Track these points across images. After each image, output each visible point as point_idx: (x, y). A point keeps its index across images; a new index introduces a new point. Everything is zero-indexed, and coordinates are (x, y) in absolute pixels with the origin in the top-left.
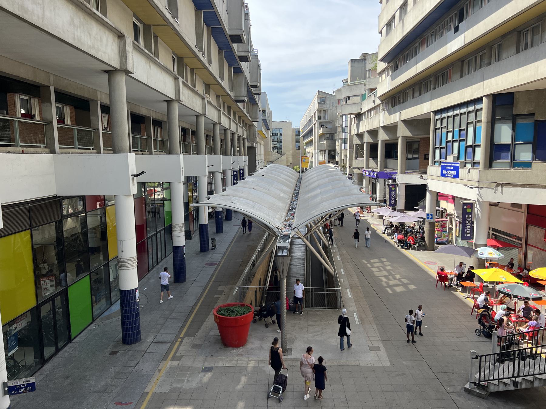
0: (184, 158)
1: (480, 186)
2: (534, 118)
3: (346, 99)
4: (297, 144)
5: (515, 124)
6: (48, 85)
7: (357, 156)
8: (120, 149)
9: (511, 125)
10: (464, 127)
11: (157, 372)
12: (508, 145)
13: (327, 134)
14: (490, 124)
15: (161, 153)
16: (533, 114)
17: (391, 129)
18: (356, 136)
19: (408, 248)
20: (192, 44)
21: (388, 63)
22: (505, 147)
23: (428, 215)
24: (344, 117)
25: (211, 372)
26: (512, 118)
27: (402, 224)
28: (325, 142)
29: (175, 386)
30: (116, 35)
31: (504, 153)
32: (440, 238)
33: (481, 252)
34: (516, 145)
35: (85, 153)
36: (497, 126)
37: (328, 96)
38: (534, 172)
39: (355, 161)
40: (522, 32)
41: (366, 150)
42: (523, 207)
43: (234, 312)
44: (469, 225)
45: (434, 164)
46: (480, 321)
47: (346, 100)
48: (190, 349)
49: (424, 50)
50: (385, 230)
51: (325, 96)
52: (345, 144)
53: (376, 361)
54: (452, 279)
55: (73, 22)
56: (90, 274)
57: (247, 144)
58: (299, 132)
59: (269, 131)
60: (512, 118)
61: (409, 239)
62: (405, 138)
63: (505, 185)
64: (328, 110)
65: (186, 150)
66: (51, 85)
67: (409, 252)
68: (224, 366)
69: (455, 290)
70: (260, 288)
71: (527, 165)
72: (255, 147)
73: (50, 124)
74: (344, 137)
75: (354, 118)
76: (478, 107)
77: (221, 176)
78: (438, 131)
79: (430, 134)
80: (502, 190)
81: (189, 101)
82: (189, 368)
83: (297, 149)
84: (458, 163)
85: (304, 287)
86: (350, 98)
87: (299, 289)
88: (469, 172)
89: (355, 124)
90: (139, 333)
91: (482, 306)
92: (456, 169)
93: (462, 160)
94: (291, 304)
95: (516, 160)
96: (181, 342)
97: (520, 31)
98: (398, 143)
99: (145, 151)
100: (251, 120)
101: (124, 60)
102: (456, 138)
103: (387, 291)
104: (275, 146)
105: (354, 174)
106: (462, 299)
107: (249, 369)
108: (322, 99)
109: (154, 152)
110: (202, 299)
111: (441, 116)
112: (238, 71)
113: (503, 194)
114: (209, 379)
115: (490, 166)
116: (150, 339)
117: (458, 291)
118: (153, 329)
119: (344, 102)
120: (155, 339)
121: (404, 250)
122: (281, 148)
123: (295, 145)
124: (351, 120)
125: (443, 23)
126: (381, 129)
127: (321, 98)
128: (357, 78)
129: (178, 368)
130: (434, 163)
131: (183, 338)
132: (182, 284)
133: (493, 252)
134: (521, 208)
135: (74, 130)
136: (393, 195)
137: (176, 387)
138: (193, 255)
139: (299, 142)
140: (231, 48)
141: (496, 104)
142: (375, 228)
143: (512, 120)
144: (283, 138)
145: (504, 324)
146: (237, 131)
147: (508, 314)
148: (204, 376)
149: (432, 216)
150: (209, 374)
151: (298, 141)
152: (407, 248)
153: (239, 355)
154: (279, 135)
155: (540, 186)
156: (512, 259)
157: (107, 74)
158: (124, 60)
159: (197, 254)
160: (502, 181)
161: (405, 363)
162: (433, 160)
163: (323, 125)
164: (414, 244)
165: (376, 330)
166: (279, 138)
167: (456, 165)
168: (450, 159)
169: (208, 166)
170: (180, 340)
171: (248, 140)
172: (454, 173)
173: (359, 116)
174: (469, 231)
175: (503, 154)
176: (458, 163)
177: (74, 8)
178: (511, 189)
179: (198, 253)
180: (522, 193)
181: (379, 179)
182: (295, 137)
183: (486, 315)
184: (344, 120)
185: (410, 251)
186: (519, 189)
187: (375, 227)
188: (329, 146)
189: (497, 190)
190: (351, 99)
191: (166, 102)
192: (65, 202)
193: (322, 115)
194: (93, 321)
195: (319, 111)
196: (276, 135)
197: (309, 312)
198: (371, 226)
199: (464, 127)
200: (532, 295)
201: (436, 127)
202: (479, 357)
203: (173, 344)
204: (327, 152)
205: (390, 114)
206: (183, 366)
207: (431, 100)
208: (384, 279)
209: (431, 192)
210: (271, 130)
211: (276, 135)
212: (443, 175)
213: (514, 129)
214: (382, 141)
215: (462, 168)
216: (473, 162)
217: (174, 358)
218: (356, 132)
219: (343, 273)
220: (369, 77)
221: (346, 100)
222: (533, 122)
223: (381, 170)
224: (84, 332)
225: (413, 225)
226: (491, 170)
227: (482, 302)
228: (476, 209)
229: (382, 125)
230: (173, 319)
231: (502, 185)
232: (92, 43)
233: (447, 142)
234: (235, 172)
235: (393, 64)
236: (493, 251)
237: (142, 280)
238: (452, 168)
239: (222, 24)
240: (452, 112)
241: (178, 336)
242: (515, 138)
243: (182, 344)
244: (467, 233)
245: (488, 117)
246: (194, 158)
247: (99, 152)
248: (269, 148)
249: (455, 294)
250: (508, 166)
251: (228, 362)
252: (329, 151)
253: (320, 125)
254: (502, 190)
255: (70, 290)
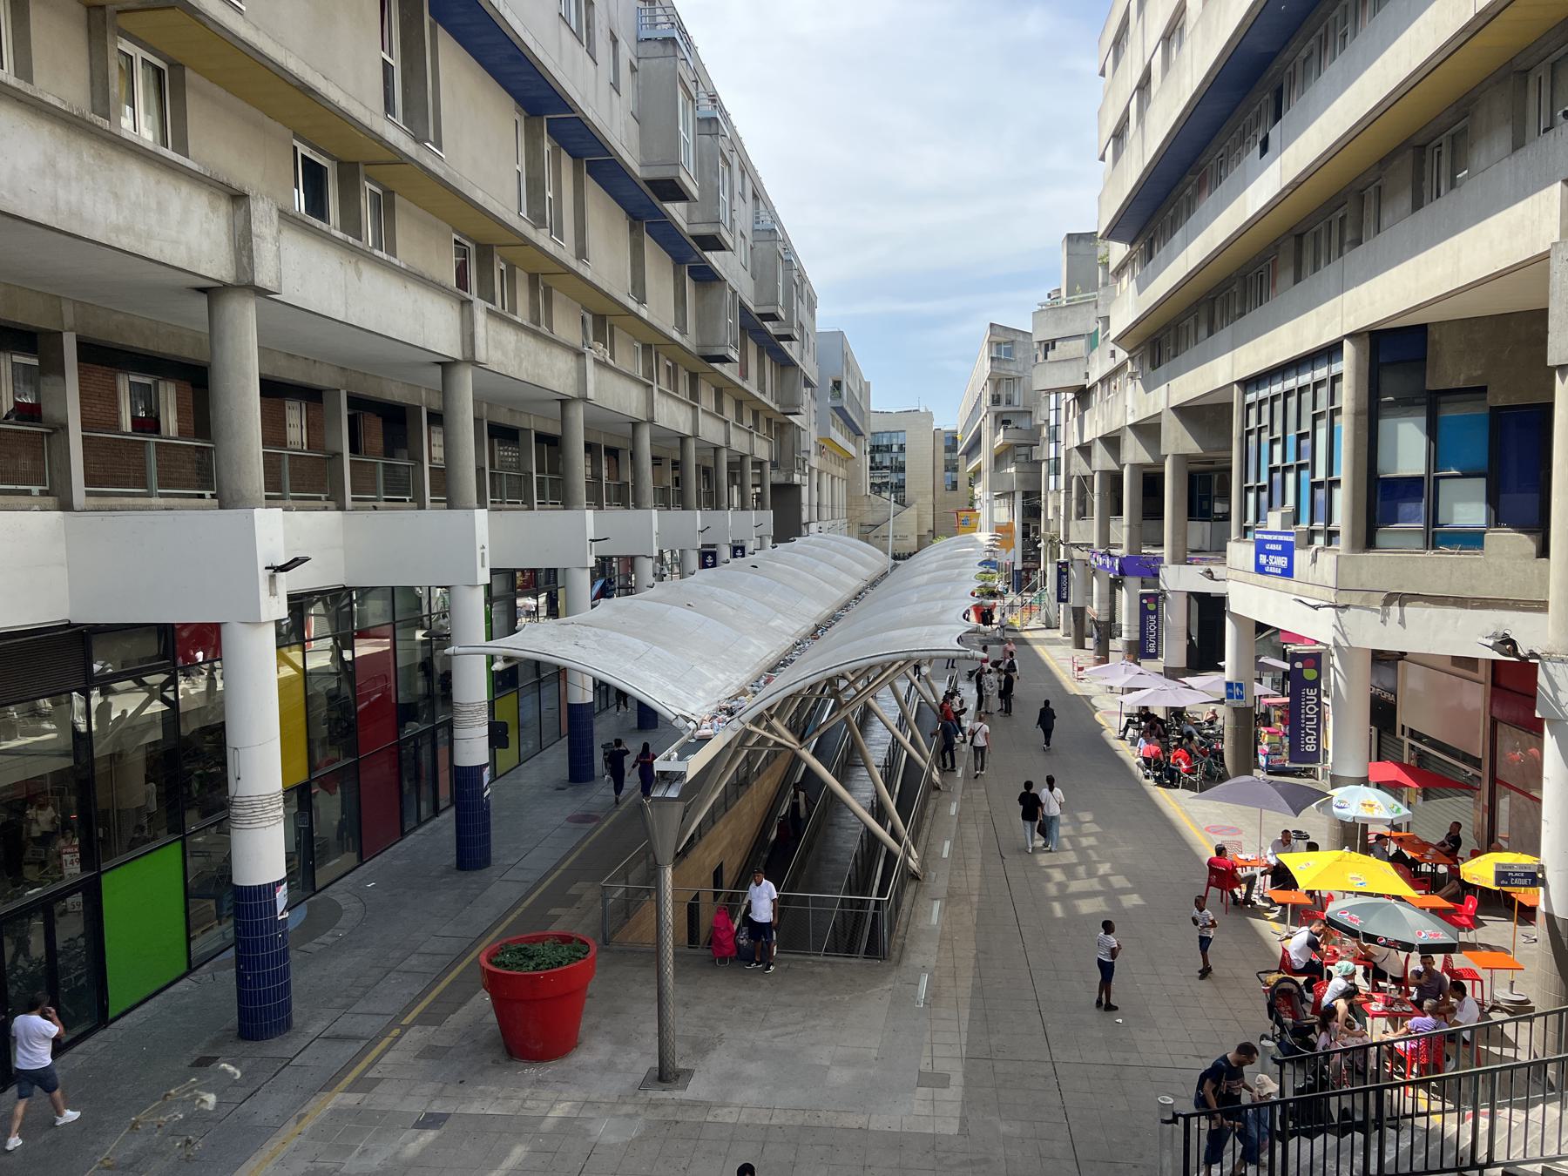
0: (490, 520)
1: (1340, 603)
2: (1485, 399)
3: (1047, 346)
4: (948, 474)
5: (1436, 419)
6: (54, 327)
7: (1081, 509)
8: (235, 498)
9: (1423, 420)
10: (1306, 427)
11: (291, 1124)
12: (1418, 480)
13: (1019, 446)
14: (1365, 418)
15: (514, 506)
16: (1483, 389)
17: (1148, 430)
18: (1078, 454)
19: (1173, 784)
20: (501, 209)
21: (1131, 245)
22: (1411, 487)
23: (1229, 685)
24: (1053, 397)
25: (438, 1127)
26: (1424, 400)
27: (1178, 713)
28: (1013, 470)
29: (322, 1165)
30: (220, 193)
31: (1408, 504)
32: (1278, 757)
33: (1341, 802)
34: (1441, 481)
35: (182, 508)
36: (1384, 424)
37: (1021, 338)
38: (1491, 560)
39: (1077, 525)
40: (1428, 151)
41: (1100, 494)
42: (1482, 667)
43: (531, 958)
44: (1312, 719)
45: (1245, 537)
46: (1272, 1009)
47: (1047, 350)
48: (411, 1061)
49: (1206, 203)
50: (1126, 729)
51: (1013, 338)
52: (1056, 474)
53: (921, 1118)
54: (1251, 881)
55: (54, 166)
56: (183, 840)
57: (772, 477)
58: (955, 439)
59: (861, 439)
60: (1424, 400)
61: (1175, 758)
62: (1182, 459)
63: (1411, 601)
64: (1020, 378)
65: (595, 501)
66: (66, 328)
67: (1176, 801)
68: (483, 1112)
69: (1259, 913)
70: (716, 895)
71: (1471, 540)
72: (798, 487)
73: (61, 431)
74: (1052, 455)
75: (1074, 399)
76: (1336, 368)
77: (654, 566)
78: (1253, 438)
79: (1231, 450)
80: (1402, 614)
81: (521, 363)
82: (383, 1113)
83: (950, 488)
84: (1292, 534)
85: (777, 891)
86: (1057, 344)
87: (762, 899)
88: (1314, 560)
89: (1076, 419)
90: (287, 1007)
91: (1302, 966)
92: (1287, 550)
93: (1304, 525)
94: (741, 942)
95: (1442, 526)
96: (398, 1038)
97: (1424, 146)
98: (1163, 473)
99: (405, 500)
100: (777, 409)
101: (245, 260)
102: (1291, 461)
103: (1051, 911)
104: (884, 480)
105: (1075, 563)
106: (1269, 943)
107: (547, 1125)
108: (1003, 346)
109: (539, 503)
110: (510, 920)
111: (1257, 396)
112: (707, 277)
113: (1405, 628)
114: (423, 1150)
115: (1370, 543)
116: (315, 1029)
117: (1266, 918)
118: (339, 1000)
119: (1041, 357)
120: (332, 1028)
121: (1160, 788)
122: (900, 487)
123: (943, 477)
124: (1067, 404)
125: (1241, 128)
126: (1129, 431)
127: (999, 344)
128: (1078, 288)
129: (356, 1113)
130: (1245, 531)
131: (405, 1029)
132: (475, 873)
133: (1376, 800)
134: (1476, 670)
135: (147, 445)
136: (1152, 625)
137: (324, 1167)
138: (547, 790)
139: (955, 469)
140: (664, 215)
141: (1381, 361)
142: (1103, 723)
143: (1425, 407)
144: (908, 459)
145: (1337, 1025)
146: (728, 442)
147: (1350, 991)
148: (414, 1139)
149: (1241, 688)
150: (431, 1135)
151: (952, 467)
152: (1172, 783)
153: (540, 1082)
154: (895, 448)
155: (1511, 603)
156: (1457, 826)
157: (206, 296)
158: (245, 260)
159: (558, 789)
160: (1401, 587)
161: (1004, 1128)
162: (1241, 525)
163: (1008, 422)
164: (1191, 772)
165: (965, 1027)
166: (897, 458)
167: (1287, 538)
168: (1274, 521)
169: (593, 541)
170: (396, 1032)
171: (774, 465)
172: (1282, 561)
173: (1083, 395)
174: (1312, 738)
175: (1406, 508)
176: (1292, 534)
177: (58, 130)
178: (1428, 610)
179: (561, 786)
180: (1459, 624)
181: (1127, 579)
182: (942, 456)
183: (1290, 991)
184: (1053, 406)
185: (1179, 793)
186: (1451, 612)
187: (1106, 720)
188: (1023, 481)
189: (1388, 614)
190: (1059, 348)
191: (440, 367)
192: (98, 645)
193: (1003, 392)
194: (191, 969)
195: (996, 380)
196: (889, 448)
197: (793, 965)
198: (1097, 716)
199: (1306, 427)
200: (1423, 935)
201: (1247, 426)
202: (1181, 1120)
203: (374, 1042)
204: (1019, 497)
205: (1147, 390)
206: (372, 1108)
207: (1233, 349)
208: (1058, 875)
209: (1238, 619)
210: (868, 435)
211: (889, 448)
212: (1260, 569)
213: (1432, 432)
214: (1133, 466)
215: (1303, 549)
216: (1329, 531)
217: (357, 1086)
218: (1077, 443)
219: (945, 855)
220: (1105, 284)
221: (1047, 350)
222: (1487, 411)
223: (1130, 551)
224: (152, 1002)
225: (1211, 715)
226: (1372, 554)
227: (1299, 952)
228: (1332, 669)
229: (1131, 421)
230: (405, 972)
231: (1403, 599)
232: (125, 218)
233: (1272, 470)
234: (710, 557)
235: (1142, 246)
236: (1375, 794)
237: (378, 857)
238: (1279, 548)
239: (612, 151)
240: (1281, 385)
241: (396, 1022)
242: (1435, 458)
243: (395, 1047)
244: (1306, 744)
245: (1357, 399)
246: (676, 515)
247: (422, 507)
248: (861, 487)
249: (1256, 926)
250: (1419, 541)
251: (500, 1101)
252: (1026, 495)
253: (1000, 421)
254: (1402, 614)
255: (105, 879)
